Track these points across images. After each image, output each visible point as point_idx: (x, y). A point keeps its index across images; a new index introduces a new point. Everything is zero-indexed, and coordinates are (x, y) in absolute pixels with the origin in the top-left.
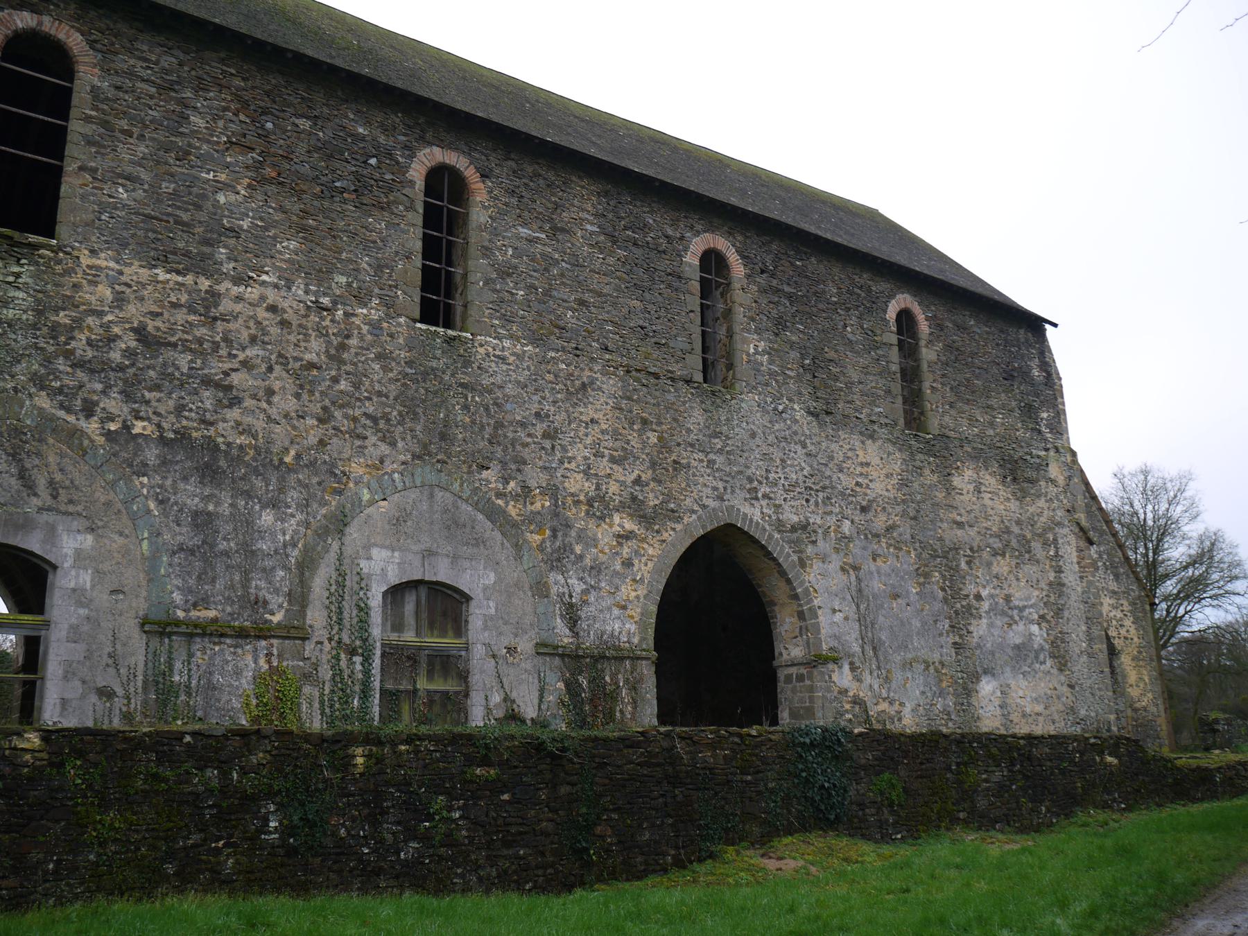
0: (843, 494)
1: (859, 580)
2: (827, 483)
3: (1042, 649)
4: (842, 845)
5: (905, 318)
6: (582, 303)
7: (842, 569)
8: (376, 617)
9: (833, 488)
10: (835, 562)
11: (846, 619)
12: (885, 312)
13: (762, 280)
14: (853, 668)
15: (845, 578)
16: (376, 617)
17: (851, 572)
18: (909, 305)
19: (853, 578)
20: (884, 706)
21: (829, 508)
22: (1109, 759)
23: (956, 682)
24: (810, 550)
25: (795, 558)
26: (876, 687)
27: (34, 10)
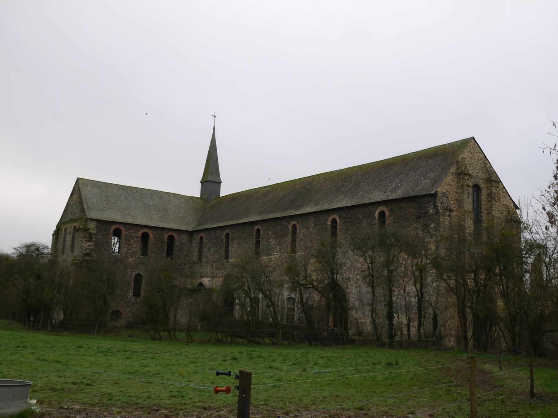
0: (358, 269)
1: (360, 290)
2: (354, 267)
3: (414, 305)
4: (423, 353)
5: (382, 214)
6: (311, 241)
7: (356, 287)
8: (286, 303)
9: (356, 267)
10: (355, 285)
11: (356, 299)
12: (374, 214)
13: (343, 221)
14: (356, 311)
15: (356, 289)
16: (286, 303)
17: (358, 288)
18: (384, 210)
19: (358, 289)
20: (362, 320)
21: (355, 273)
22: (325, 333)
23: (383, 315)
24: (349, 284)
25: (345, 286)
26: (361, 315)
27: (494, 301)
